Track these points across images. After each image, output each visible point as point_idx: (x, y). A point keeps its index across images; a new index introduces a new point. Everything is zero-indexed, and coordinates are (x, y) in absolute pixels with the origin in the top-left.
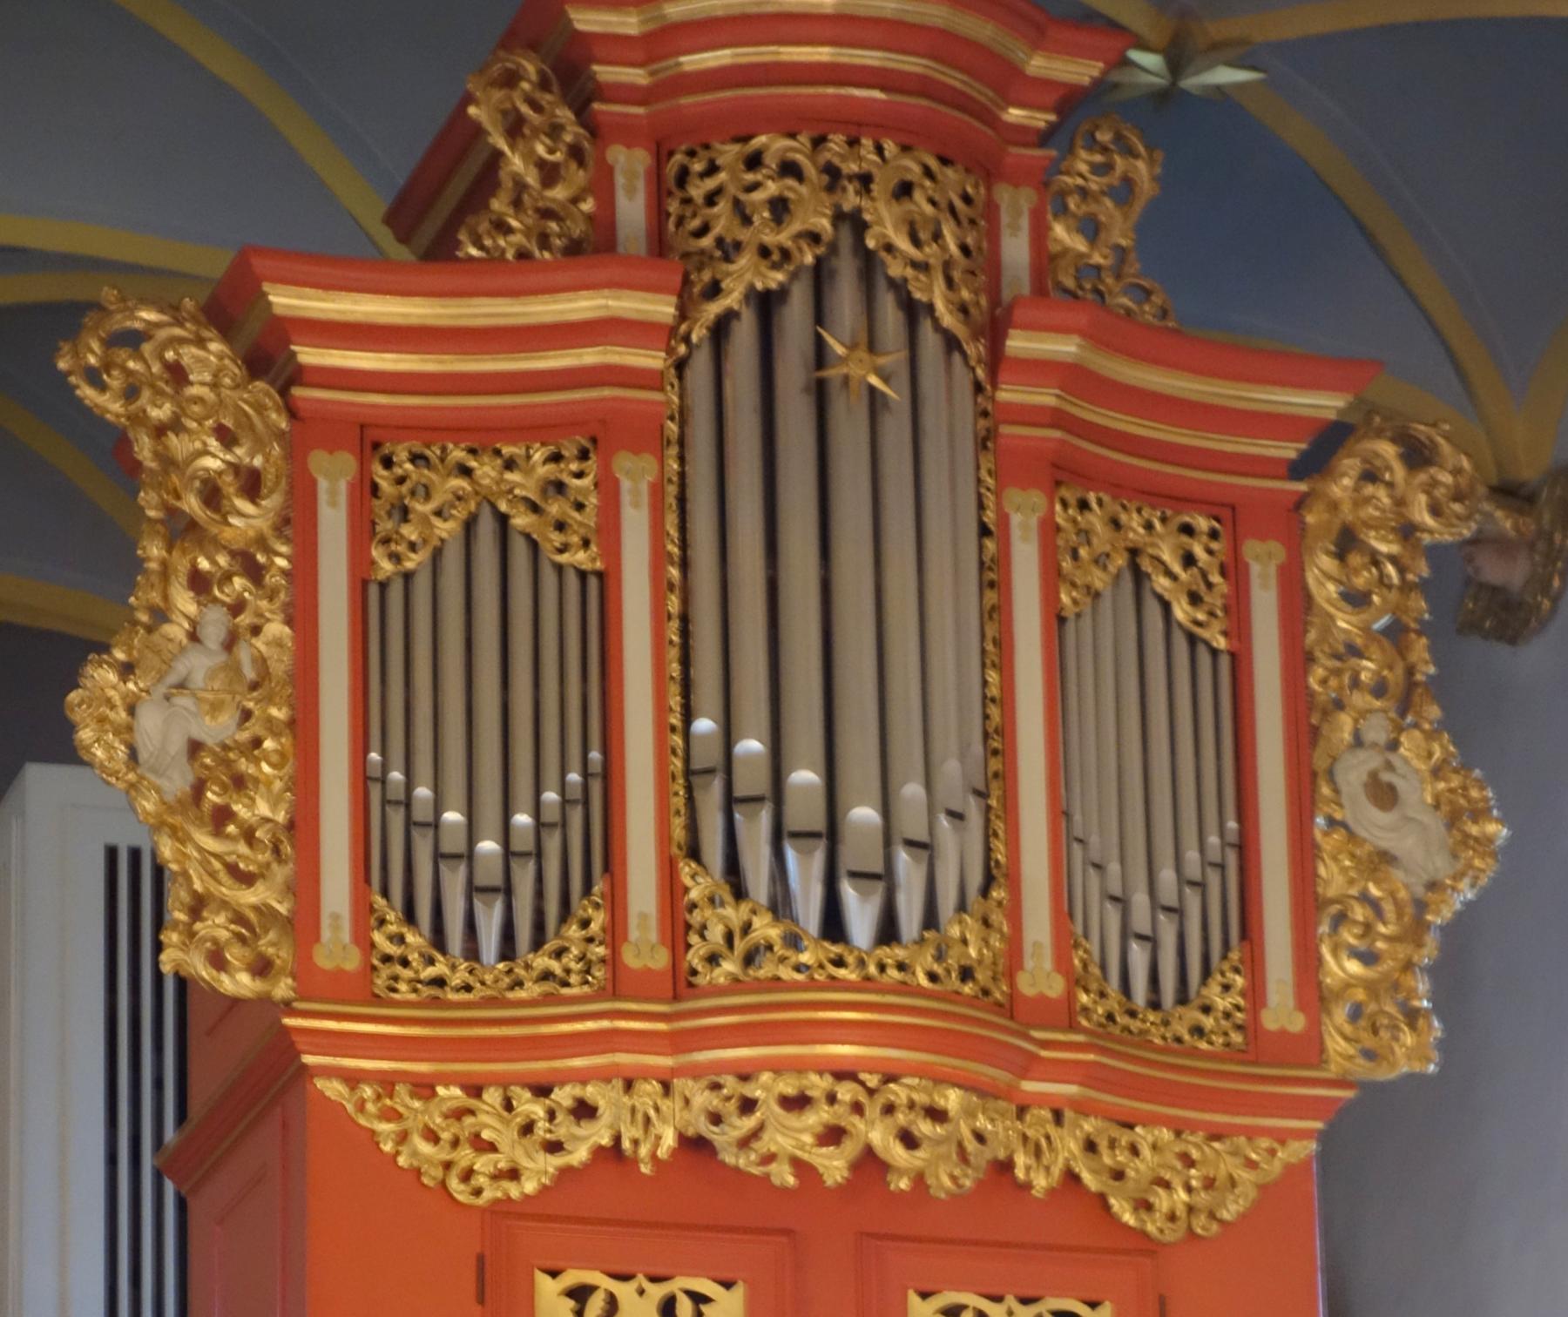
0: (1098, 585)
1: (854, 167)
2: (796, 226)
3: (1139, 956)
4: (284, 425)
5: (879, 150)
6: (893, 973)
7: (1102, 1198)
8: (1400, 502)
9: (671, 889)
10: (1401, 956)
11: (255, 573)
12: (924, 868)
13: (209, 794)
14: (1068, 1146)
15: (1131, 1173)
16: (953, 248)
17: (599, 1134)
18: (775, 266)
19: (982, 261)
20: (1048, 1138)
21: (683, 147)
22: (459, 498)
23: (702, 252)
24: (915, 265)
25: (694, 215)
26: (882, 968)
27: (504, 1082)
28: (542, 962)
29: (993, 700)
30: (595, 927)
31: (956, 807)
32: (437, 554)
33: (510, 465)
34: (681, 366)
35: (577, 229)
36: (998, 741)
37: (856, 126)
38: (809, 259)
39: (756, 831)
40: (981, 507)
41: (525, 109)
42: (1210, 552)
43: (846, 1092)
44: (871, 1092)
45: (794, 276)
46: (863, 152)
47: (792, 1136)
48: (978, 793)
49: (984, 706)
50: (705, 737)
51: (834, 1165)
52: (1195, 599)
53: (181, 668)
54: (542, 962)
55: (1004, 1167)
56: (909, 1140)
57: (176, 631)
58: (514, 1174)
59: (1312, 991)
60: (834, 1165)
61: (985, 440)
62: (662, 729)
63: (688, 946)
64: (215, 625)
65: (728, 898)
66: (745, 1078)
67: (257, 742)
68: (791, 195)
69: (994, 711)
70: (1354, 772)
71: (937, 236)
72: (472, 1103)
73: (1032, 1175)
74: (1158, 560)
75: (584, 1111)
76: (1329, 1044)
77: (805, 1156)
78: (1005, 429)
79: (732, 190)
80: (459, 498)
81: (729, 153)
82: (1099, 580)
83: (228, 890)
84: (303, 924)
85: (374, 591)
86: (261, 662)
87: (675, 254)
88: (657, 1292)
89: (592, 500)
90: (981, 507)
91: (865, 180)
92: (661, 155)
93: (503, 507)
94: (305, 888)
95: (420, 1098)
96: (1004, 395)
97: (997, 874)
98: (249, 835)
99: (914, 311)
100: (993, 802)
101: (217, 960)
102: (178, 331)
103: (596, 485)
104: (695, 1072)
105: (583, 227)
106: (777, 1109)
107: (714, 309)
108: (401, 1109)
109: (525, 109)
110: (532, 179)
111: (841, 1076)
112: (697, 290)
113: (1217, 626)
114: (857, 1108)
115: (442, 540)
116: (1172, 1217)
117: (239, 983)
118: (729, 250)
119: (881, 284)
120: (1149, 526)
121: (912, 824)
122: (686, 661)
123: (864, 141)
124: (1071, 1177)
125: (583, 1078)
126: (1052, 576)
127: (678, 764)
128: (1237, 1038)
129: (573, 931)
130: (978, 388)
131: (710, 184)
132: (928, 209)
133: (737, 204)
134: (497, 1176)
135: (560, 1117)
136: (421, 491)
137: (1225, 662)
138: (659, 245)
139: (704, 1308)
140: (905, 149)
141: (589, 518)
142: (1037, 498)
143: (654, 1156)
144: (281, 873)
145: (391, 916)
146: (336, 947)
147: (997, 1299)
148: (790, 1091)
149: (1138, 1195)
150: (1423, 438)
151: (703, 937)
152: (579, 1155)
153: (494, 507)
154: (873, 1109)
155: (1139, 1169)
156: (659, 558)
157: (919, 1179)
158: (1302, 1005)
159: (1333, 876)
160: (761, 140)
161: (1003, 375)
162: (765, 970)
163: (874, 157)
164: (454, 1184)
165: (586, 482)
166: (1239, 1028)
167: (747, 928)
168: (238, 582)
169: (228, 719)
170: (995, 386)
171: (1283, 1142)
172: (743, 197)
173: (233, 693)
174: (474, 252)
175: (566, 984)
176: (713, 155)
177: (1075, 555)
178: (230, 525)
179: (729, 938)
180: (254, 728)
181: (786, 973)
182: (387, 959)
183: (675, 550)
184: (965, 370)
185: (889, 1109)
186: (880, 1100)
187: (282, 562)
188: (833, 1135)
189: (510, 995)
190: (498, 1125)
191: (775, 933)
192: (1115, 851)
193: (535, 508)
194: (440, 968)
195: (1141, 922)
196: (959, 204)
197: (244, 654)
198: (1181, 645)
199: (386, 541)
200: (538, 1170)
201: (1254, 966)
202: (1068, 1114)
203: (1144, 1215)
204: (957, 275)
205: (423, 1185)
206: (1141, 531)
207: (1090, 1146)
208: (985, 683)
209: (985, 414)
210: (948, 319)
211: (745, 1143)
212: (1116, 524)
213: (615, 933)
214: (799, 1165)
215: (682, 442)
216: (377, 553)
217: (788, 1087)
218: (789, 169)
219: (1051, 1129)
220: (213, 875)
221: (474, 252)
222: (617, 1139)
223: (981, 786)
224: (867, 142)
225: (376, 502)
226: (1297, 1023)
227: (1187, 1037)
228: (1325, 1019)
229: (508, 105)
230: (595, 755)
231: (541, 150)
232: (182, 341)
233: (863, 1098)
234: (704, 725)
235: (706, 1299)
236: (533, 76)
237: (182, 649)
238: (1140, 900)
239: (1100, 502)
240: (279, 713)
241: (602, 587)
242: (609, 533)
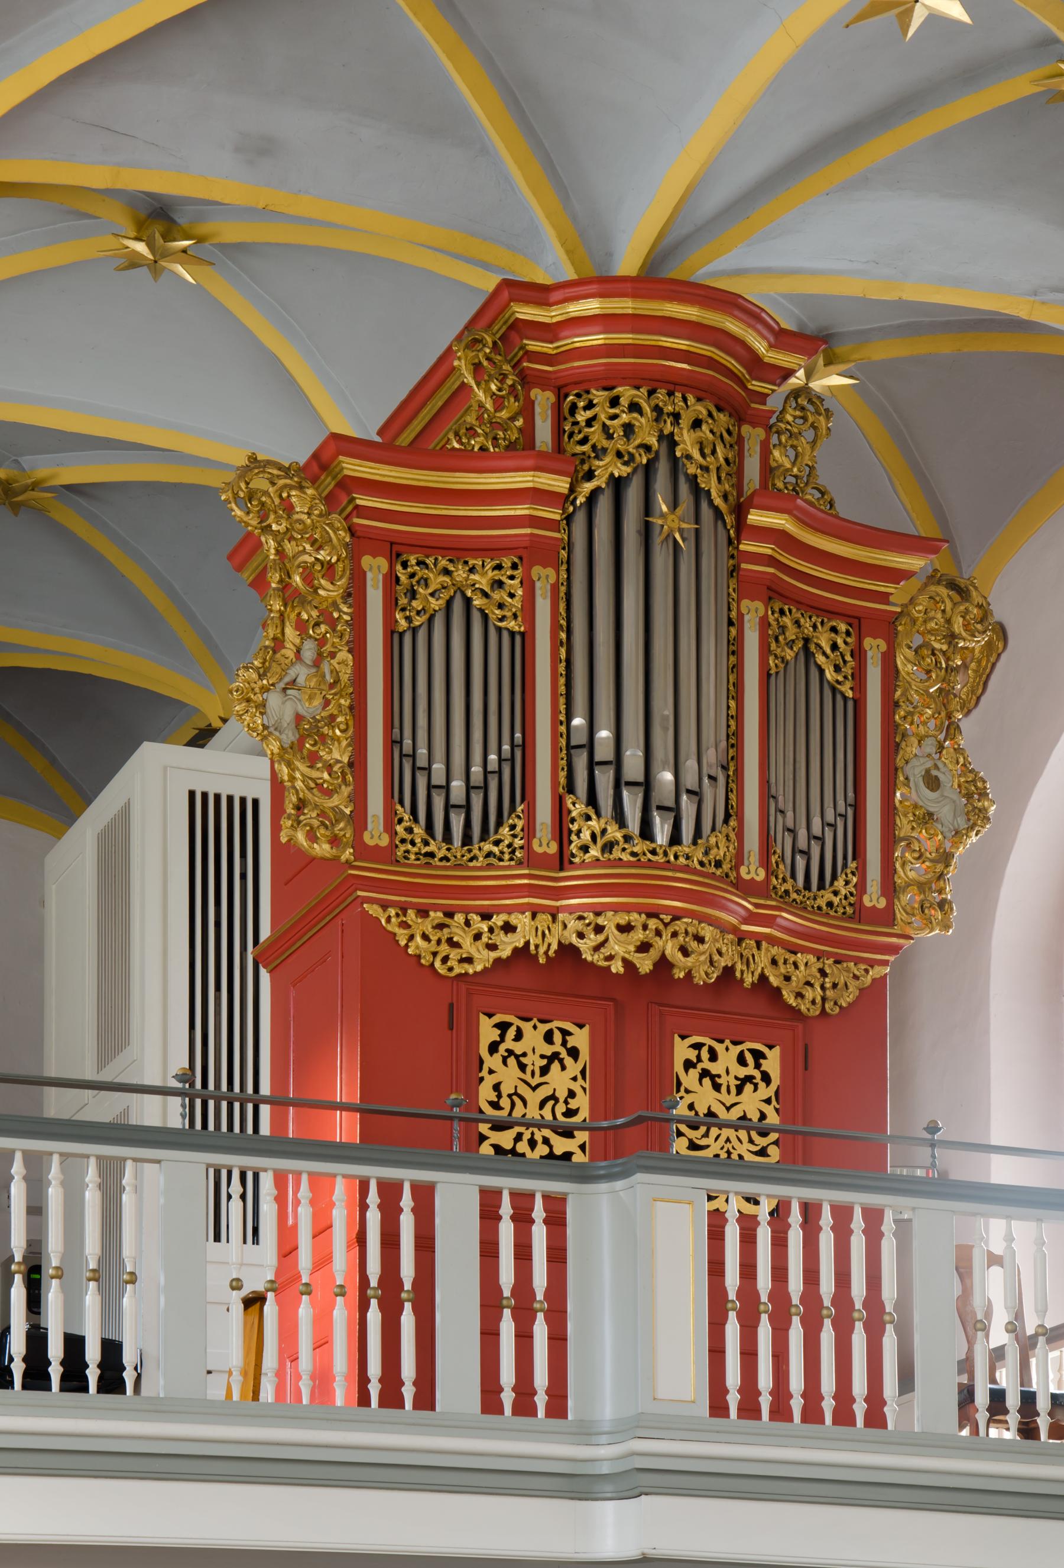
0: (788, 658)
1: (670, 408)
2: (638, 442)
3: (800, 862)
4: (348, 540)
5: (685, 400)
6: (682, 860)
7: (778, 990)
8: (948, 621)
9: (560, 812)
10: (938, 870)
11: (333, 623)
12: (695, 806)
13: (307, 746)
14: (762, 961)
15: (794, 978)
16: (721, 459)
17: (517, 940)
18: (626, 463)
19: (735, 468)
20: (753, 956)
21: (575, 392)
22: (444, 588)
23: (584, 453)
24: (701, 467)
25: (580, 432)
26: (676, 857)
27: (466, 911)
28: (488, 847)
29: (732, 717)
30: (518, 829)
31: (713, 774)
32: (431, 620)
33: (472, 570)
34: (569, 519)
35: (514, 436)
36: (735, 740)
37: (674, 384)
38: (644, 461)
39: (605, 780)
40: (729, 610)
41: (485, 363)
42: (846, 643)
43: (653, 924)
44: (666, 925)
45: (635, 470)
46: (676, 401)
47: (620, 947)
48: (723, 767)
49: (728, 721)
50: (576, 727)
51: (645, 964)
52: (837, 669)
53: (292, 673)
54: (488, 847)
55: (729, 971)
56: (685, 951)
57: (289, 652)
58: (469, 960)
59: (890, 889)
60: (645, 964)
61: (732, 571)
62: (555, 723)
63: (571, 842)
64: (309, 652)
65: (594, 817)
66: (598, 914)
67: (332, 718)
68: (637, 424)
69: (732, 723)
70: (916, 770)
71: (714, 452)
72: (448, 921)
73: (745, 975)
74: (818, 645)
75: (509, 928)
76: (898, 916)
77: (630, 958)
78: (743, 566)
79: (603, 417)
80: (444, 588)
81: (599, 396)
82: (789, 654)
83: (316, 798)
84: (359, 819)
85: (396, 637)
86: (335, 672)
87: (568, 455)
88: (543, 1028)
89: (520, 592)
90: (729, 610)
91: (676, 417)
92: (561, 396)
93: (469, 593)
94: (359, 798)
95: (422, 917)
96: (742, 547)
97: (732, 813)
98: (329, 768)
99: (698, 492)
100: (731, 773)
101: (312, 837)
102: (288, 481)
103: (521, 582)
104: (571, 910)
105: (516, 435)
106: (616, 932)
107: (588, 487)
108: (410, 922)
109: (485, 363)
110: (489, 405)
111: (650, 915)
112: (581, 475)
113: (848, 684)
114: (658, 933)
115: (435, 611)
116: (813, 1002)
117: (322, 849)
118: (599, 452)
119: (682, 480)
120: (815, 627)
121: (690, 780)
122: (569, 685)
123: (677, 394)
124: (763, 978)
125: (509, 910)
126: (765, 651)
127: (563, 742)
128: (849, 910)
129: (505, 831)
130: (730, 542)
131: (589, 414)
132: (710, 436)
133: (605, 428)
134: (462, 960)
135: (496, 931)
136: (422, 582)
137: (850, 704)
138: (559, 447)
139: (568, 1038)
140: (699, 400)
141: (517, 603)
142: (759, 605)
143: (546, 953)
144: (346, 791)
145: (406, 817)
146: (376, 835)
147: (721, 1041)
148: (623, 922)
149: (797, 990)
150: (963, 586)
151: (579, 837)
152: (505, 952)
153: (463, 594)
154: (667, 934)
155: (799, 976)
156: (555, 628)
157: (689, 975)
158: (884, 894)
159: (904, 826)
160: (620, 389)
161: (743, 535)
162: (617, 853)
163: (682, 404)
164: (438, 964)
165: (516, 582)
166: (851, 904)
167: (604, 832)
168: (323, 628)
169: (318, 702)
170: (739, 543)
171: (872, 967)
172: (608, 422)
173: (321, 690)
174: (457, 446)
175: (501, 860)
176: (591, 397)
177: (777, 640)
178: (319, 595)
179: (594, 837)
180: (332, 709)
181: (626, 857)
182: (403, 841)
183: (564, 623)
184: (724, 531)
185: (675, 935)
186: (671, 929)
187: (347, 618)
188: (644, 947)
189: (471, 864)
190: (462, 933)
191: (619, 836)
192: (791, 805)
193: (485, 595)
194: (433, 847)
195: (802, 843)
196: (725, 435)
197: (326, 667)
198: (828, 693)
199: (403, 610)
200: (483, 959)
201: (861, 871)
202: (764, 944)
203: (799, 1000)
204: (723, 475)
205: (422, 965)
206: (811, 629)
207: (774, 962)
208: (728, 707)
209: (732, 557)
210: (718, 501)
211: (597, 949)
212: (797, 623)
213: (530, 831)
214: (626, 962)
215: (568, 562)
216: (398, 616)
217: (623, 919)
218: (634, 407)
219: (755, 951)
220: (310, 789)
221: (457, 446)
222: (527, 943)
223: (725, 764)
224: (679, 395)
225: (398, 588)
226: (882, 903)
227: (825, 908)
228: (896, 902)
229: (476, 361)
230: (518, 735)
231: (493, 387)
232: (291, 487)
233: (661, 927)
234: (577, 721)
235: (570, 1034)
236: (490, 345)
237: (292, 663)
238: (802, 833)
239: (790, 611)
240: (345, 702)
241: (526, 640)
242: (529, 609)
